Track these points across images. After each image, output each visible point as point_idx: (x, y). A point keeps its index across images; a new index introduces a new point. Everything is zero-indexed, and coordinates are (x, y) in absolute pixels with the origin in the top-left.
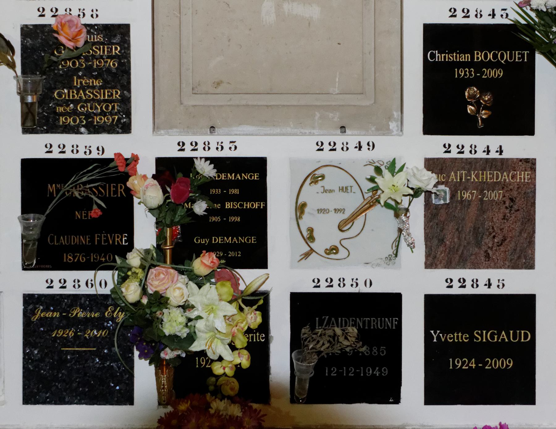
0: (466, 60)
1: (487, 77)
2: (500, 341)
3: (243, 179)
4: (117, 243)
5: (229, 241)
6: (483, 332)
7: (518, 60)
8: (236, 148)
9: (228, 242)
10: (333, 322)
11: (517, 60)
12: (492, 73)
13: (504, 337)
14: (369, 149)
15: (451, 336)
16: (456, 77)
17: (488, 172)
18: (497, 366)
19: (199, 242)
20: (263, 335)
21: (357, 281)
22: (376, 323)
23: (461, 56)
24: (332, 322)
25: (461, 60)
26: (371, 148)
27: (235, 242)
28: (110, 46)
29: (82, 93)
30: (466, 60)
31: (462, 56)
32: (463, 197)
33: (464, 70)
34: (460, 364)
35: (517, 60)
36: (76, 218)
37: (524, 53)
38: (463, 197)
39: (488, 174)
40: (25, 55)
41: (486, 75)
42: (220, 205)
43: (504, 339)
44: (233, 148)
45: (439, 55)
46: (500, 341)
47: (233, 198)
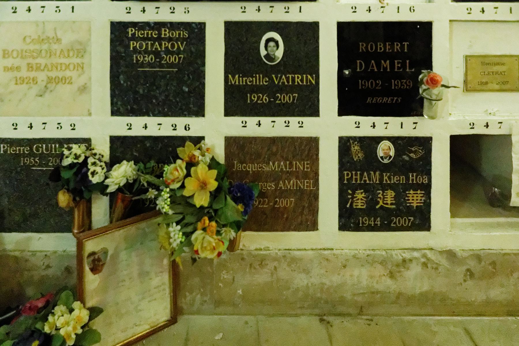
0: (258, 83)
1: (167, 62)
2: (280, 84)
3: (309, 84)
4: (362, 50)
5: (235, 82)
6: (304, 76)
7: (398, 70)
8: (60, 11)
9: (233, 83)
10: (373, 64)
11: (396, 70)
12: (287, 98)
13: (374, 67)
14: (413, 7)
15: (27, 148)
16: (249, 102)
17: (306, 162)
18: (171, 61)
19: (40, 152)
20: (267, 78)
21: (188, 9)
22: (300, 80)
23: (238, 165)
24: (371, 64)
25: (238, 169)
26: (412, 8)
27: (283, 83)
28: (293, 76)
29: (158, 45)
30: (305, 83)
31: (239, 166)
32: (139, 60)
33: (257, 95)
34: (256, 99)
35: (396, 70)
36: (314, 75)
37: (289, 77)
38: (139, 60)
39: (305, 164)
40: (226, 98)
41: (166, 60)
42: (267, 80)
43: (157, 48)
44: (58, 11)
45: (248, 170)
46: (280, 84)
47: (256, 89)
